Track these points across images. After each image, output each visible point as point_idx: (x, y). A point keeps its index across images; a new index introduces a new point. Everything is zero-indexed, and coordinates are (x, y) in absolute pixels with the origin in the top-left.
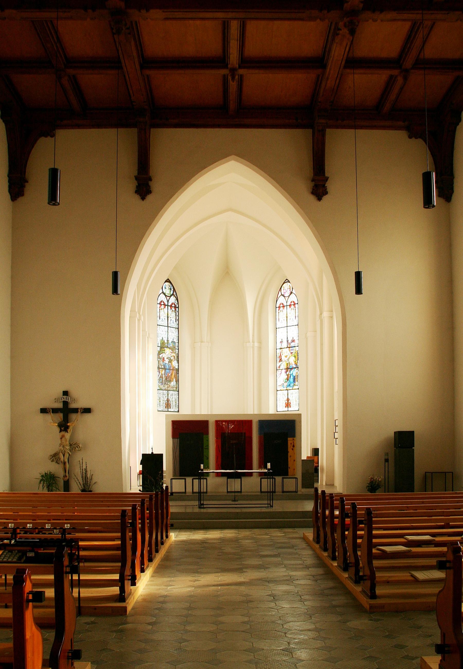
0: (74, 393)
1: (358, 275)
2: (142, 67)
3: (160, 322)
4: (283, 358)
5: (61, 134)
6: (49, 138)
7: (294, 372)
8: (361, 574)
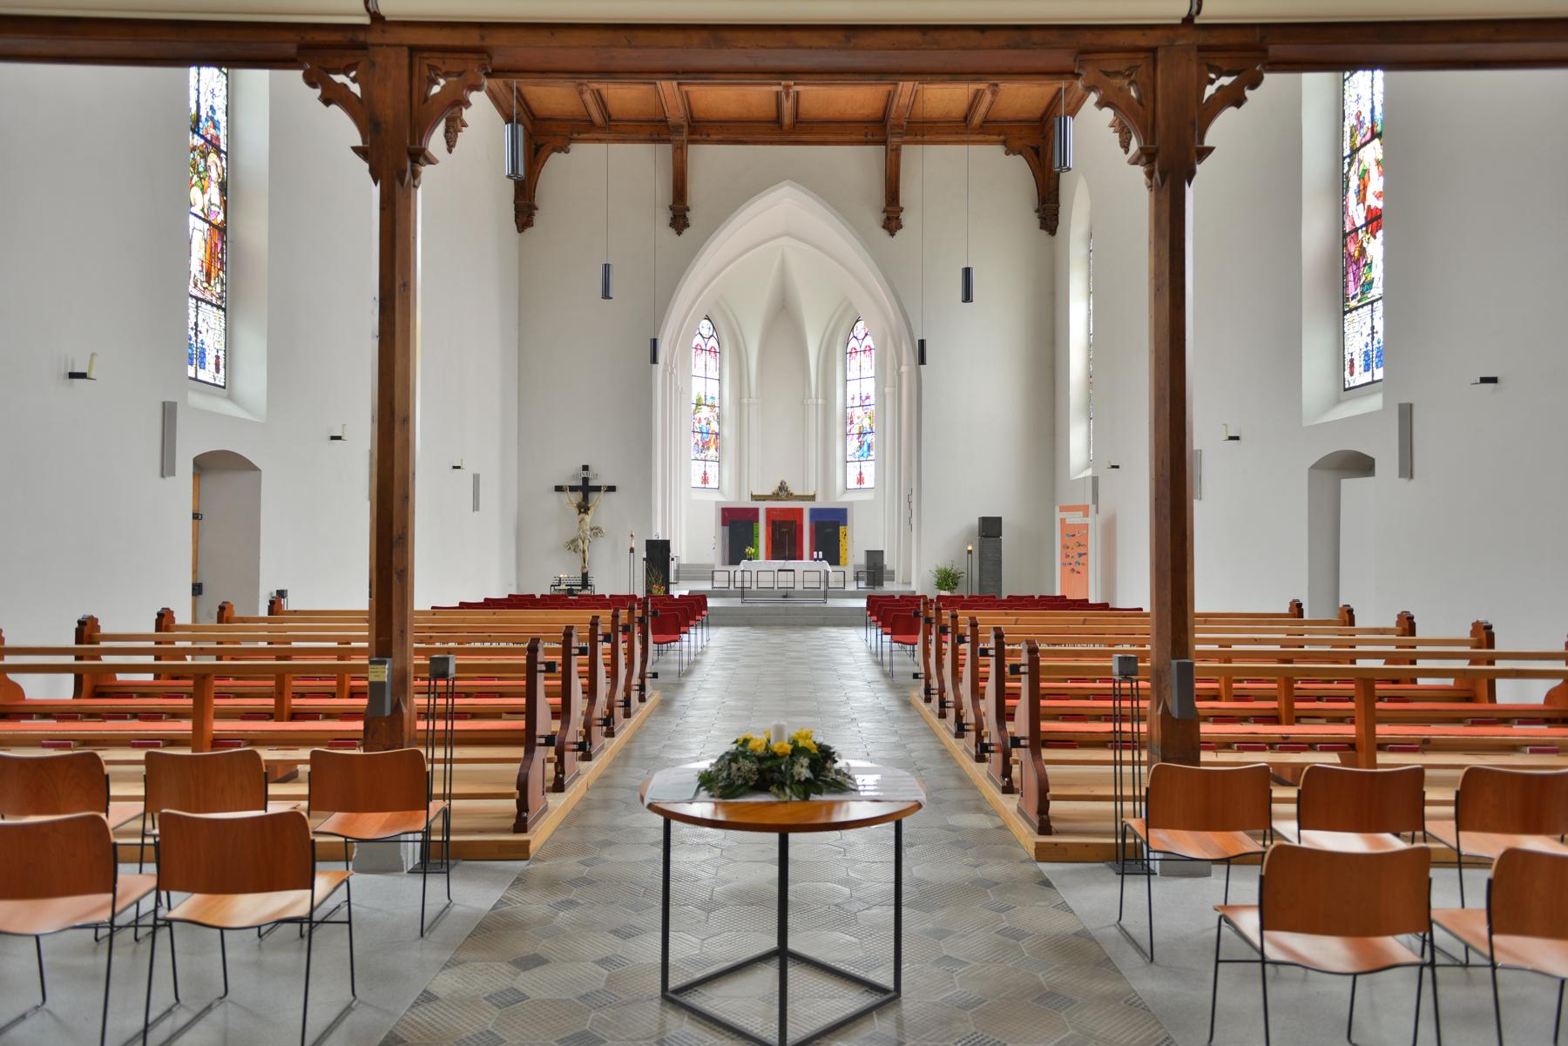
0: (594, 469)
1: (967, 272)
5: (574, 147)
7: (869, 438)
8: (986, 741)
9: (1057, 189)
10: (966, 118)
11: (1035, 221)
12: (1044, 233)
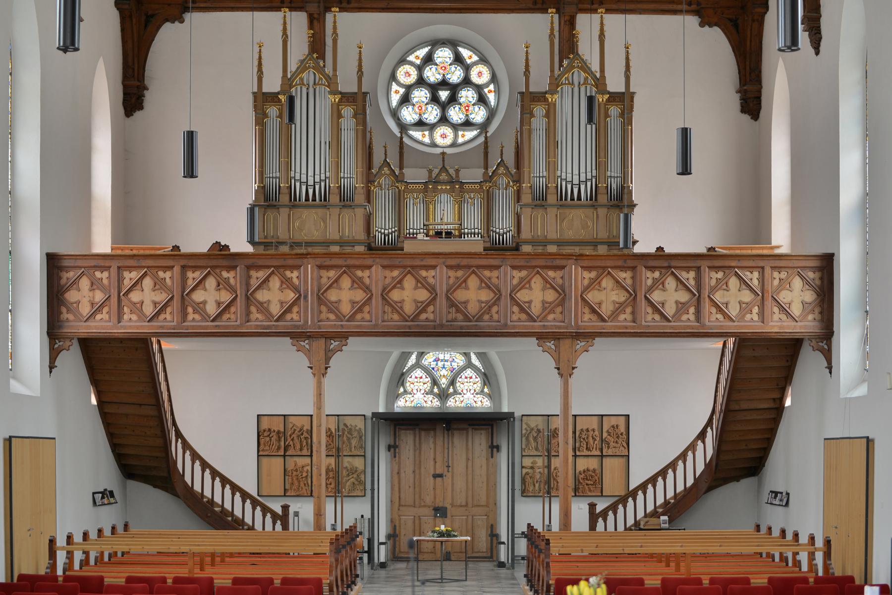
12: (746, 117)
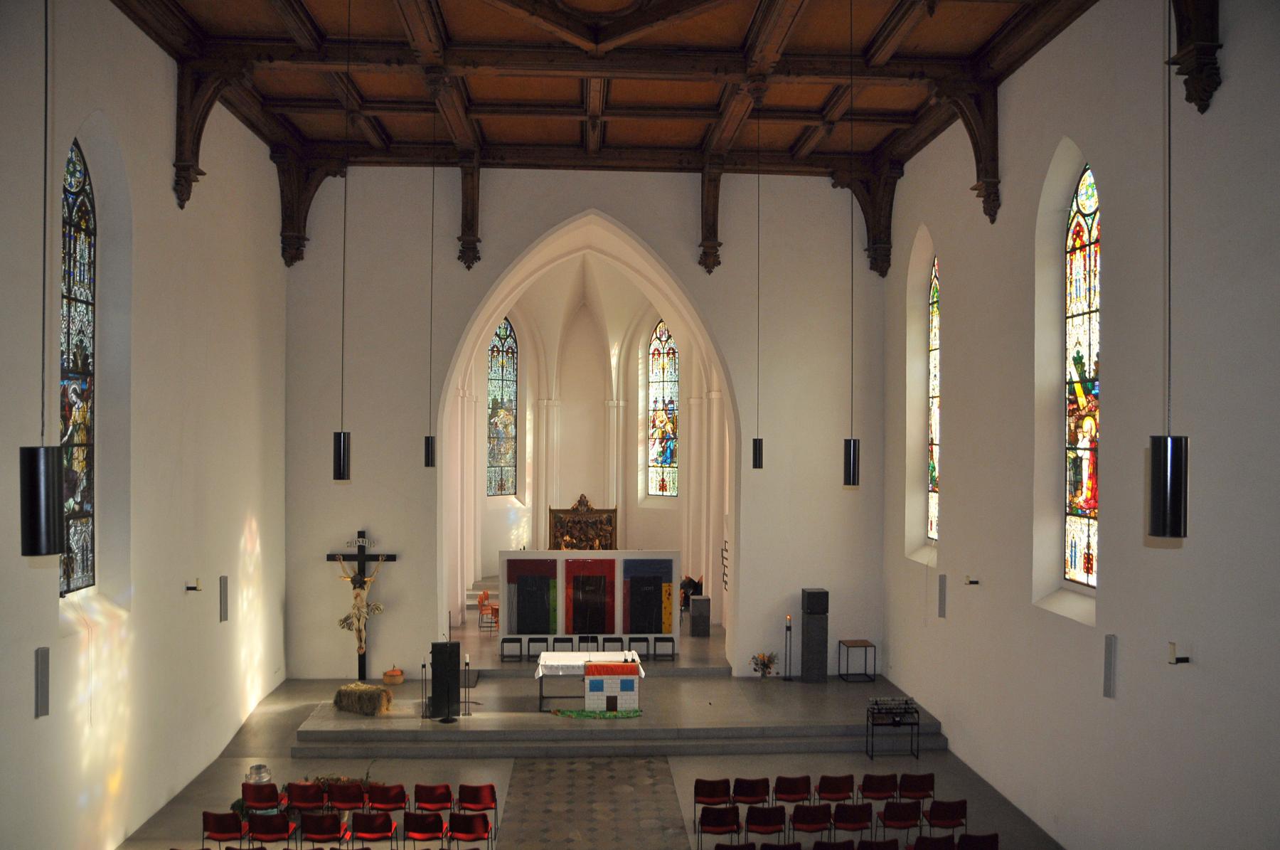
2: (467, 111)
3: (492, 375)
4: (657, 423)
5: (352, 170)
6: (338, 178)
9: (889, 228)
10: (868, 50)
11: (862, 260)
12: (875, 274)
